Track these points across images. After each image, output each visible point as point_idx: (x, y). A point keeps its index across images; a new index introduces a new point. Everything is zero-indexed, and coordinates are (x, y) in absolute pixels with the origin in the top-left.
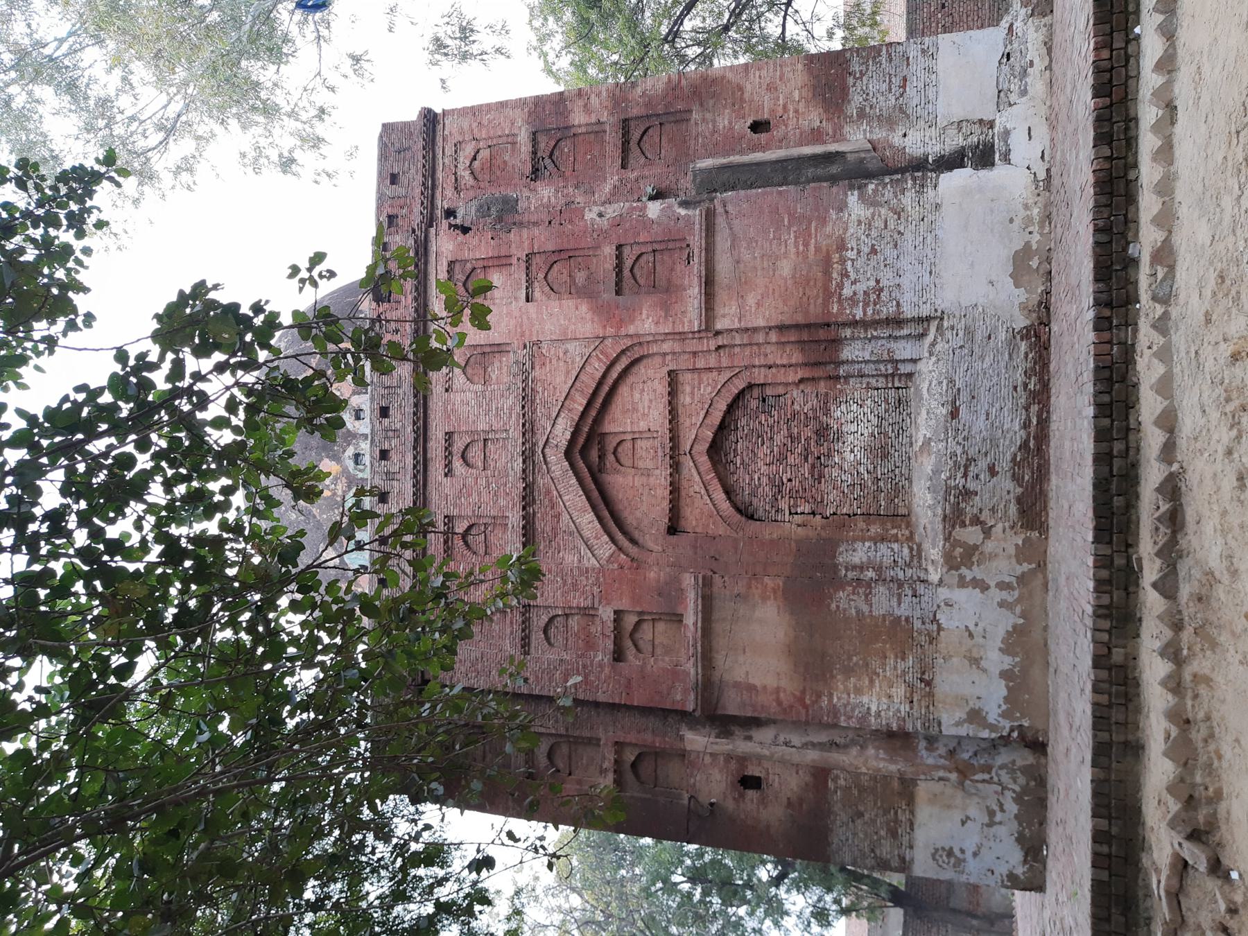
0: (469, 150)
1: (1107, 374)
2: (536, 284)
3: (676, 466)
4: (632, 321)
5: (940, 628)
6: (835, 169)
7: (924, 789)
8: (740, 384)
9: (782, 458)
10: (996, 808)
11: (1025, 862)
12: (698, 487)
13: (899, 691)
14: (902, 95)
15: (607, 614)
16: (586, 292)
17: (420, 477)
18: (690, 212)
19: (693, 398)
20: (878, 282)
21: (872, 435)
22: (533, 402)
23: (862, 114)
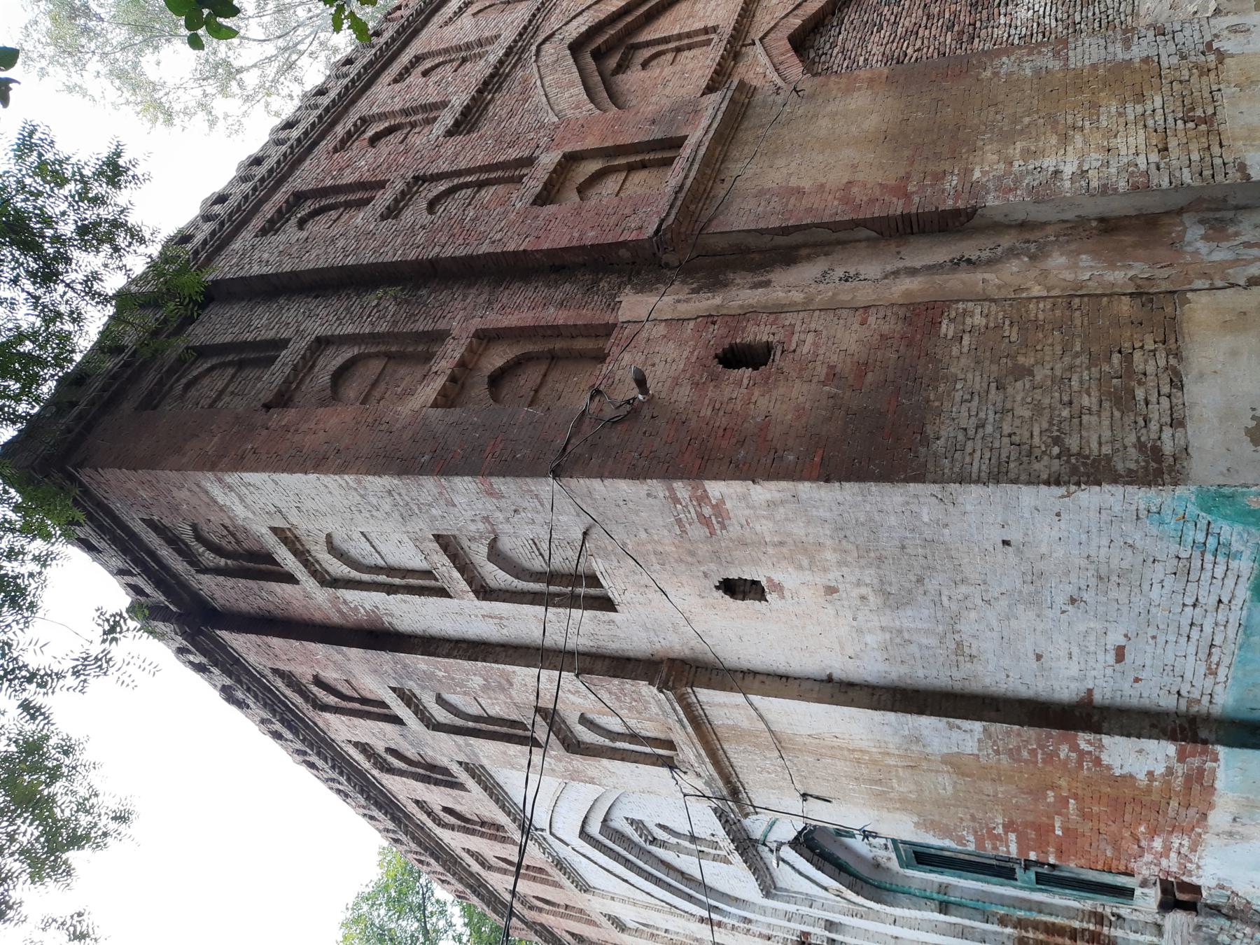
5: (1221, 56)
17: (353, 92)
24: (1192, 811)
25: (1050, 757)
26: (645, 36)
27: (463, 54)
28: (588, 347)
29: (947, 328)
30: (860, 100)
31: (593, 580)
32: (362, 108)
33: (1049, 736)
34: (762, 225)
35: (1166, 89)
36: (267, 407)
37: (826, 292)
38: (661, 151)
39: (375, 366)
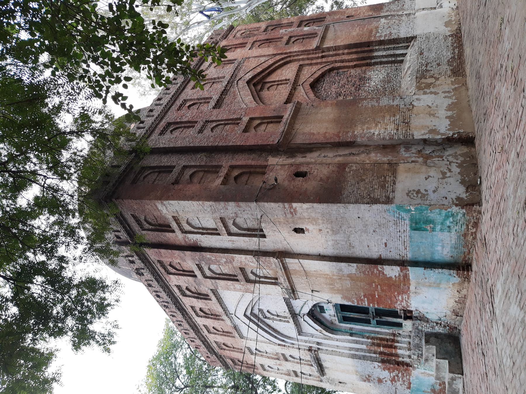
5: (413, 106)
17: (180, 91)
24: (406, 286)
25: (373, 273)
26: (268, 80)
27: (213, 81)
28: (262, 170)
29: (347, 170)
30: (329, 109)
31: (262, 230)
32: (183, 96)
33: (372, 267)
34: (304, 142)
35: (400, 114)
36: (173, 184)
37: (320, 160)
38: (278, 119)
39: (201, 174)
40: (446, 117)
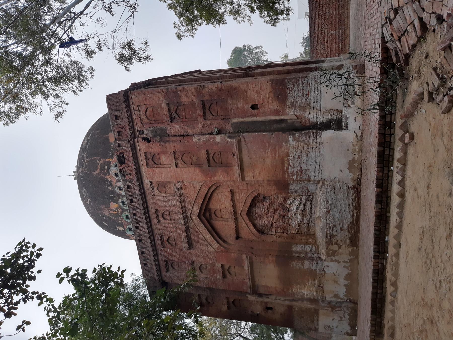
0: (143, 108)
1: (377, 271)
2: (179, 161)
3: (236, 218)
4: (215, 176)
5: (325, 273)
6: (284, 125)
7: (321, 312)
8: (255, 194)
9: (272, 216)
10: (342, 316)
11: (351, 329)
12: (244, 224)
13: (313, 289)
14: (307, 98)
15: (219, 265)
16: (198, 165)
17: (149, 223)
18: (232, 140)
19: (239, 197)
20: (301, 168)
21: (302, 210)
22: (184, 200)
23: (293, 105)
40: (344, 285)
